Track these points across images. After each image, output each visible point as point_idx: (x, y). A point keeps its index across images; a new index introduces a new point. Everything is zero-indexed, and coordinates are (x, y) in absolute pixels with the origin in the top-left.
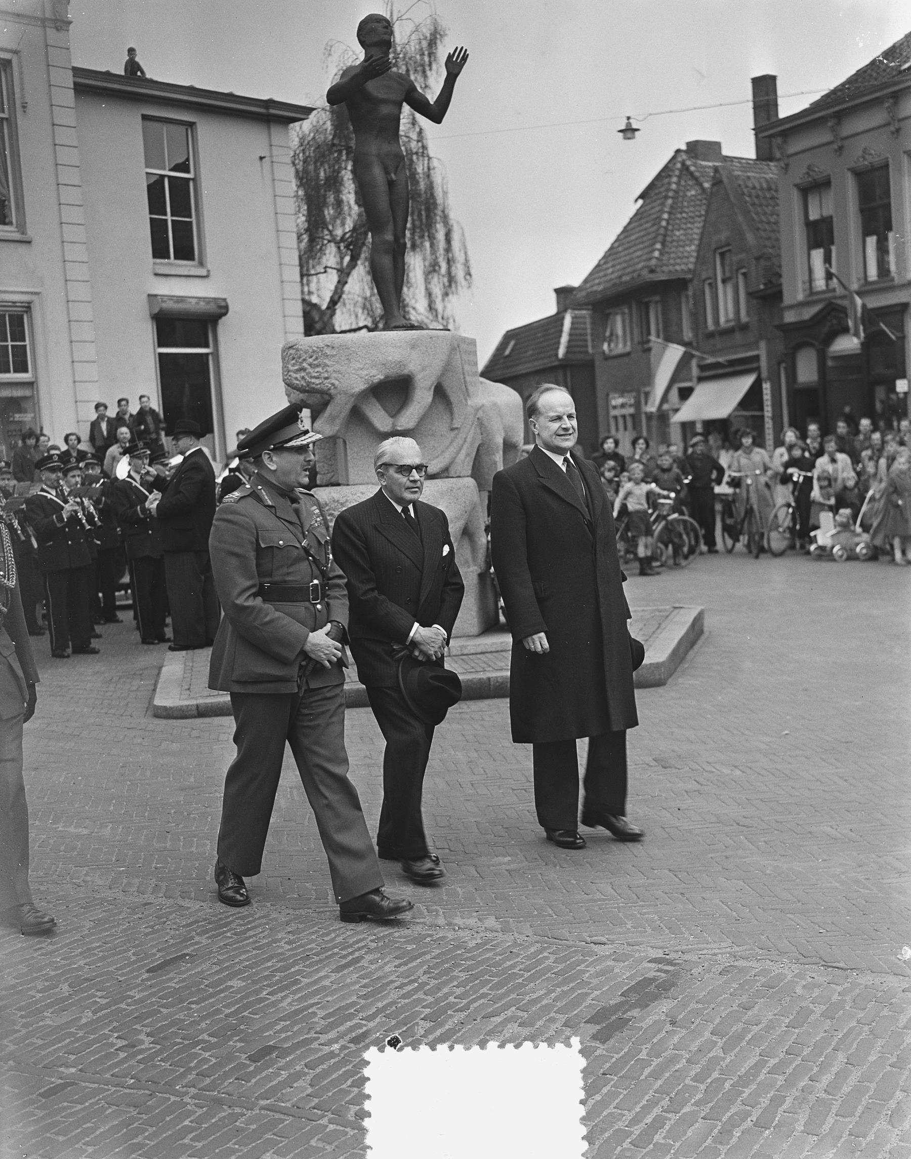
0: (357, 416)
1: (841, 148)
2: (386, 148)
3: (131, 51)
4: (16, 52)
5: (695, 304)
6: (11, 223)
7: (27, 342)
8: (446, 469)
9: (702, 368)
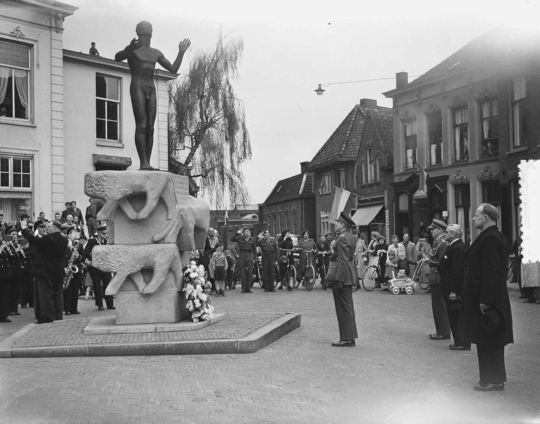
0: (119, 210)
1: (421, 104)
3: (93, 44)
4: (36, 41)
6: (27, 118)
7: (31, 173)
8: (163, 239)
9: (360, 202)
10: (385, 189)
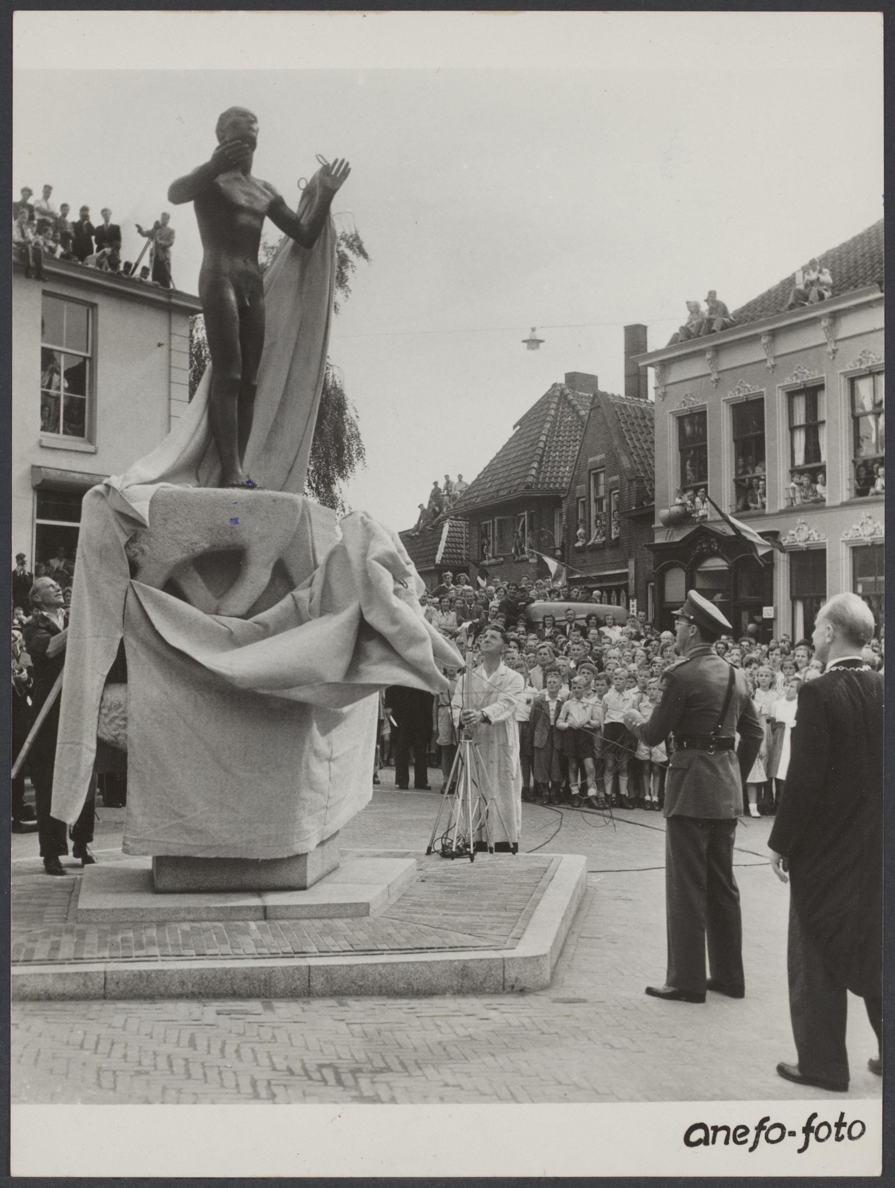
2: (239, 263)
5: (567, 520)
10: (630, 556)
